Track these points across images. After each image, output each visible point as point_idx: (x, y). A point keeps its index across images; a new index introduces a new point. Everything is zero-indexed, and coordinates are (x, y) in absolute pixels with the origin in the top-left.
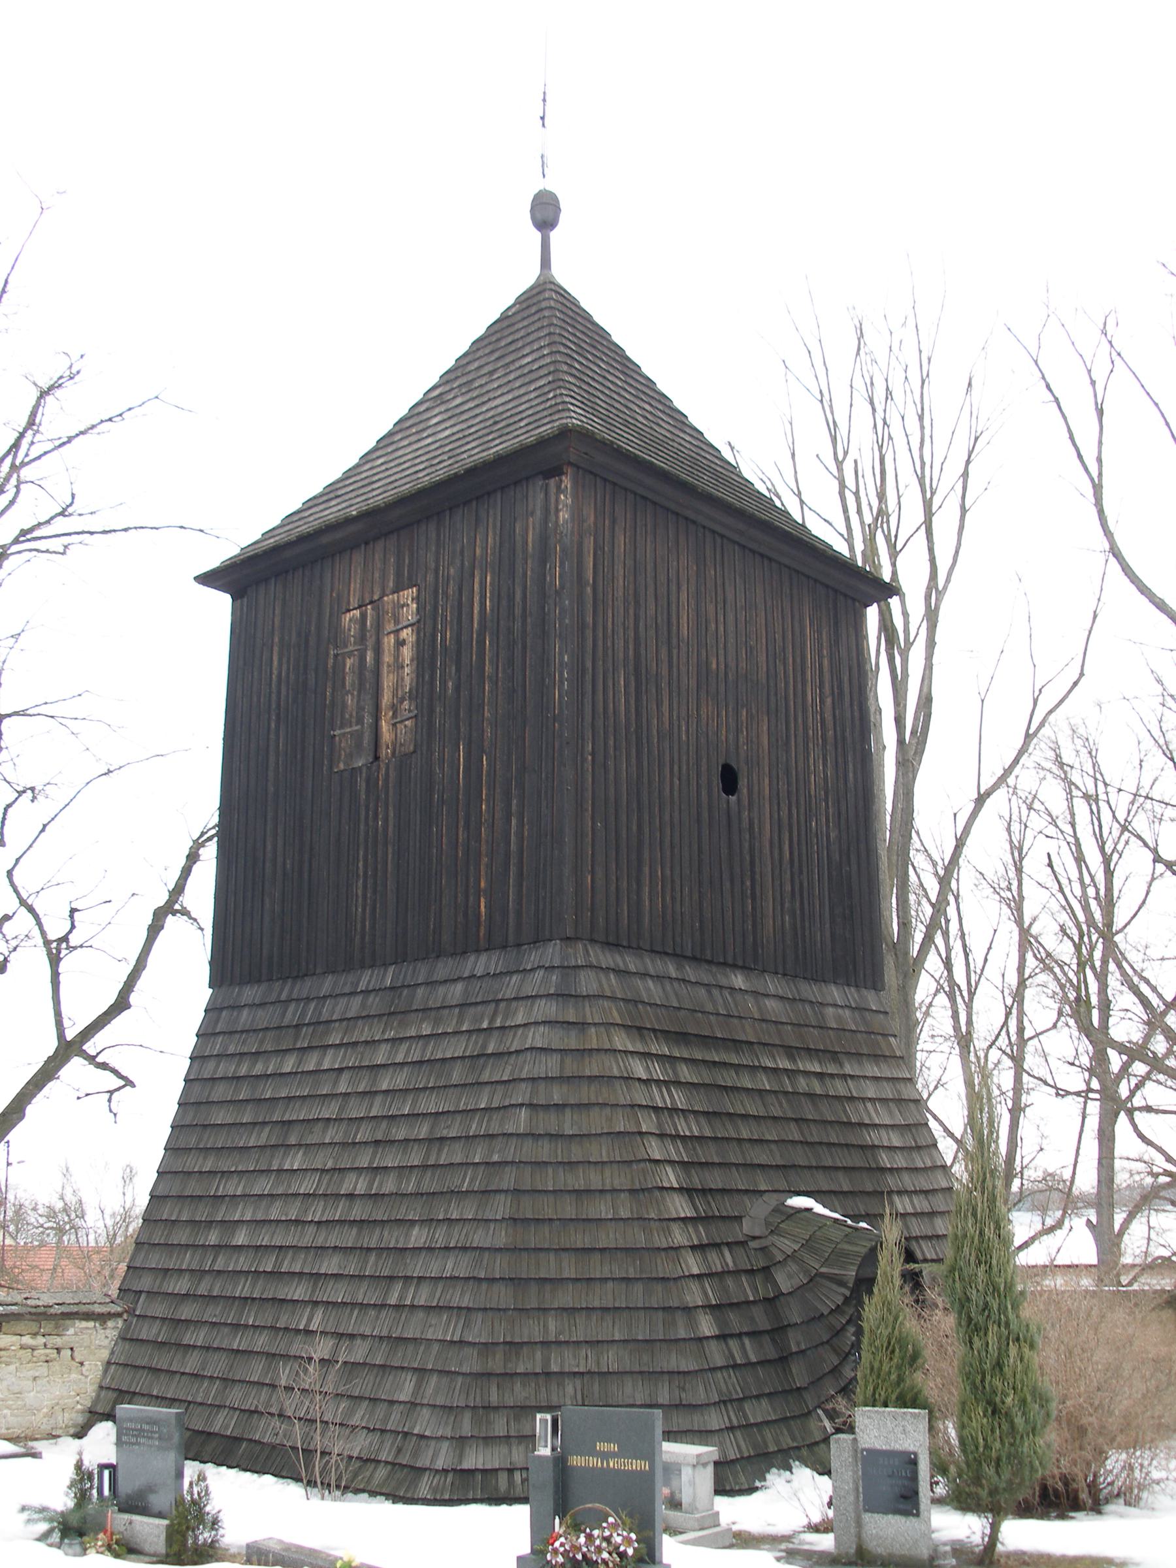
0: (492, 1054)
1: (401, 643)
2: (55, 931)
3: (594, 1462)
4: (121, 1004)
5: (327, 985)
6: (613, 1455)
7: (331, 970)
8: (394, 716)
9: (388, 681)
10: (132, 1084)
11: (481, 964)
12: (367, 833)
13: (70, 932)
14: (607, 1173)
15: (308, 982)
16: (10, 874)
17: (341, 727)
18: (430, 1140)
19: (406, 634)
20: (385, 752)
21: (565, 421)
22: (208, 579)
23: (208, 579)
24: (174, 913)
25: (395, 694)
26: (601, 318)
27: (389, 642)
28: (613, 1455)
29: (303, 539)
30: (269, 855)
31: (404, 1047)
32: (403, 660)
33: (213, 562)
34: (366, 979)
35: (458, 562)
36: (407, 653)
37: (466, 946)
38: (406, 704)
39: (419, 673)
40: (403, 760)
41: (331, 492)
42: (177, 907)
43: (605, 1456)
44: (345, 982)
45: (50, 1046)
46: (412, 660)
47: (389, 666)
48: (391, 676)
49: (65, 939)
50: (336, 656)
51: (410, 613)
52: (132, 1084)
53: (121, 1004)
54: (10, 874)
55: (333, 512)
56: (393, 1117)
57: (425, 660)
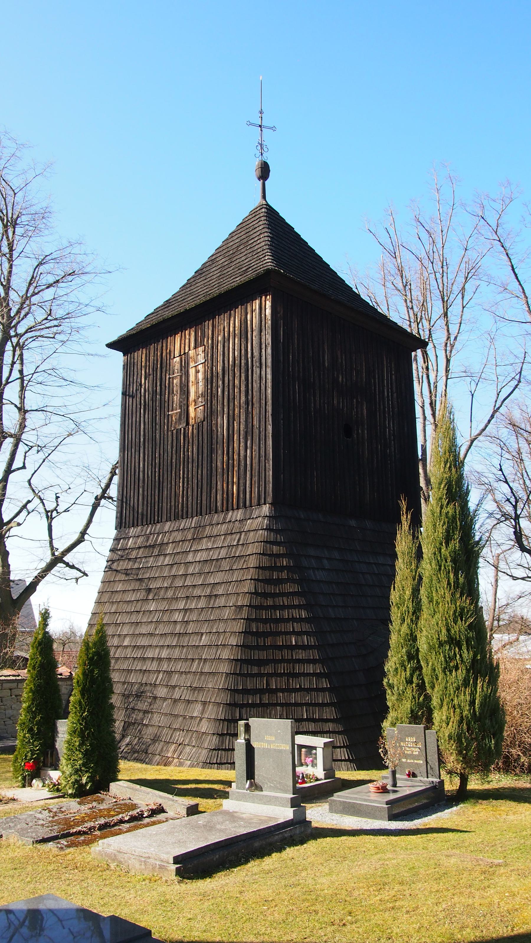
0: (238, 556)
1: (197, 372)
2: (49, 506)
3: (266, 746)
4: (80, 540)
5: (167, 526)
6: (273, 742)
7: (169, 519)
8: (195, 405)
9: (192, 390)
10: (87, 575)
11: (239, 514)
12: (184, 458)
13: (57, 507)
14: (136, 663)
15: (159, 526)
16: (29, 481)
17: (172, 411)
18: (210, 596)
19: (200, 367)
20: (192, 422)
21: (268, 267)
22: (111, 346)
23: (111, 346)
24: (105, 498)
25: (196, 395)
26: (289, 221)
27: (192, 372)
28: (273, 742)
29: (153, 326)
30: (141, 469)
31: (199, 554)
32: (199, 380)
33: (114, 338)
34: (184, 523)
35: (222, 334)
36: (200, 376)
37: (228, 508)
38: (200, 400)
39: (206, 385)
40: (199, 425)
41: (168, 304)
42: (106, 495)
43: (269, 742)
44: (175, 525)
45: (48, 558)
46: (203, 379)
47: (192, 382)
48: (193, 386)
49: (55, 509)
50: (170, 378)
51: (201, 359)
52: (87, 575)
53: (80, 540)
54: (29, 481)
55: (168, 314)
56: (195, 586)
57: (210, 380)
